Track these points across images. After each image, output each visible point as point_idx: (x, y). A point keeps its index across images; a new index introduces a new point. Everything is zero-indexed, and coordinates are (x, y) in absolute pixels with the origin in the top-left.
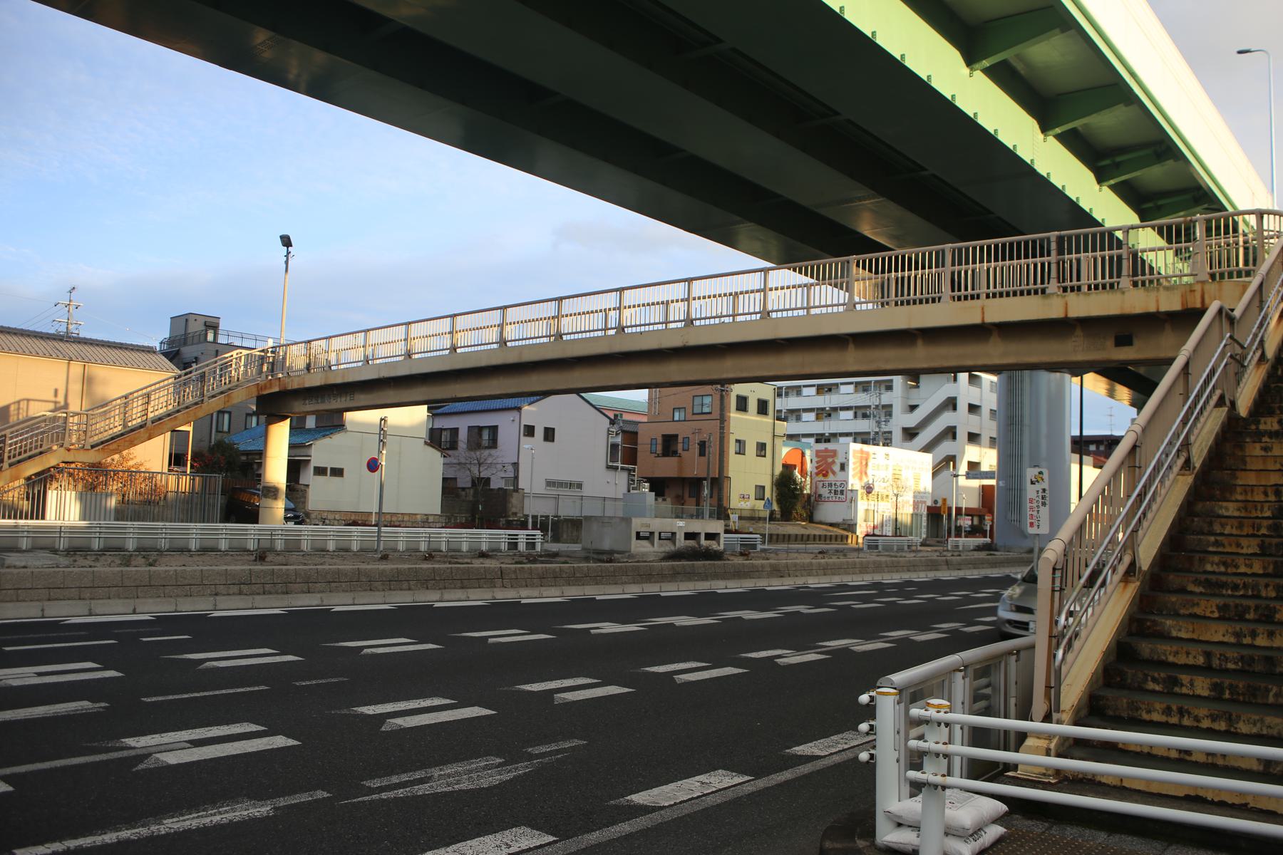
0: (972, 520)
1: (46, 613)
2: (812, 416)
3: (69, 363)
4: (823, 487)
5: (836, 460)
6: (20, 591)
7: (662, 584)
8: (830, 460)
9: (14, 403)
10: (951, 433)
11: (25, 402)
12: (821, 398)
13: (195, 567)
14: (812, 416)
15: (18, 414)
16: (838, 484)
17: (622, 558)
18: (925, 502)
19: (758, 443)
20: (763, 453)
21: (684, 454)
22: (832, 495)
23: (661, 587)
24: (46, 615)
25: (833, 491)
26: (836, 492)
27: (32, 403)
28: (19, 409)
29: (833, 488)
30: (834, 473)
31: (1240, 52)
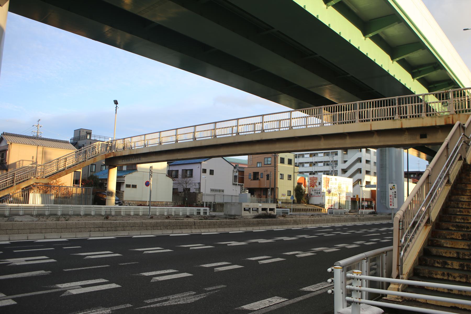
0: (368, 203)
1: (11, 240)
2: (308, 165)
3: (38, 147)
4: (312, 191)
5: (317, 181)
6: (19, 230)
7: (254, 227)
8: (315, 181)
9: (18, 161)
10: (359, 171)
11: (22, 161)
12: (311, 158)
13: (83, 221)
14: (308, 165)
15: (19, 165)
16: (318, 190)
17: (239, 218)
18: (350, 196)
19: (288, 175)
20: (290, 179)
21: (261, 179)
22: (316, 194)
23: (253, 228)
24: (29, 239)
25: (316, 193)
26: (317, 193)
27: (24, 161)
28: (19, 164)
29: (316, 191)
30: (316, 186)
31: (464, 30)
